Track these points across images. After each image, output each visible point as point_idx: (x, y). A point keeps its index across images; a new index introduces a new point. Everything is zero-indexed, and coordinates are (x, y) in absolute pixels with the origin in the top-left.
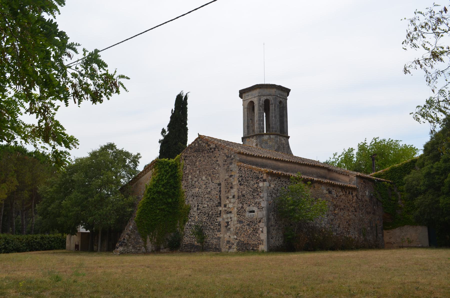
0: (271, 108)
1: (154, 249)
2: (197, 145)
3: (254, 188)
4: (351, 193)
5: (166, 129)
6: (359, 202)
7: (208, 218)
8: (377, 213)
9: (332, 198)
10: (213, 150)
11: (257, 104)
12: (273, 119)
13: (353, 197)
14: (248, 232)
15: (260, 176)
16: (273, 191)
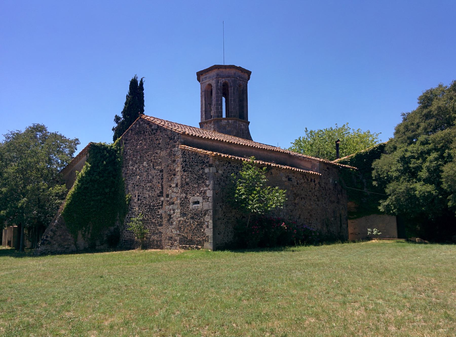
0: (229, 91)
1: (88, 247)
2: (138, 126)
3: (199, 174)
4: (313, 180)
5: (121, 116)
6: (322, 191)
7: (150, 210)
8: (341, 202)
9: (292, 186)
10: (154, 131)
11: (215, 87)
12: (232, 102)
13: (315, 185)
14: (192, 226)
15: (206, 161)
16: (222, 178)
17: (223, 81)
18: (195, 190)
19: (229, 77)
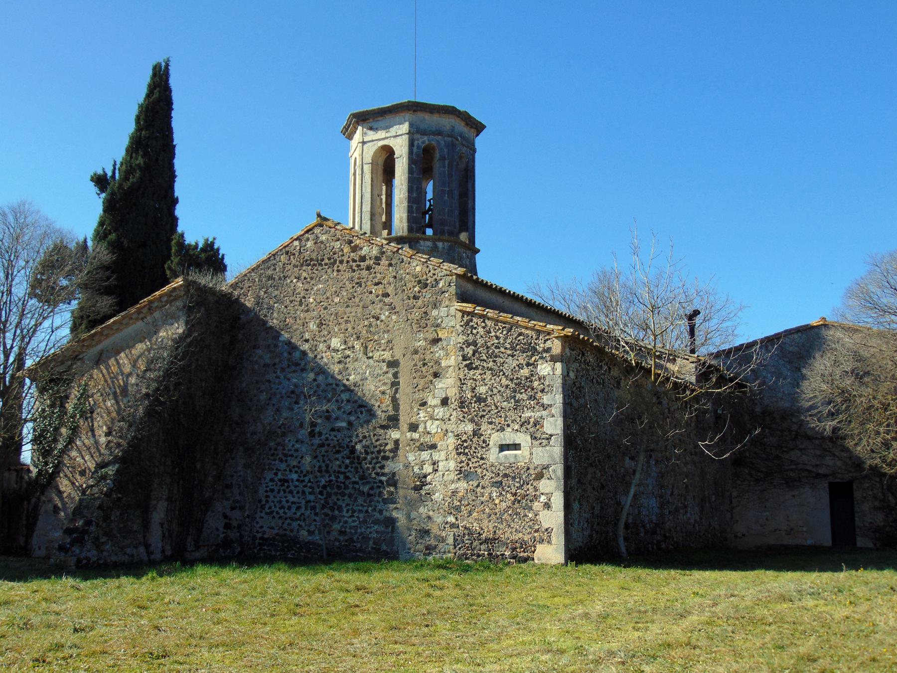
7: (352, 463)
15: (542, 345)
17: (423, 142)
18: (506, 416)
19: (438, 133)
